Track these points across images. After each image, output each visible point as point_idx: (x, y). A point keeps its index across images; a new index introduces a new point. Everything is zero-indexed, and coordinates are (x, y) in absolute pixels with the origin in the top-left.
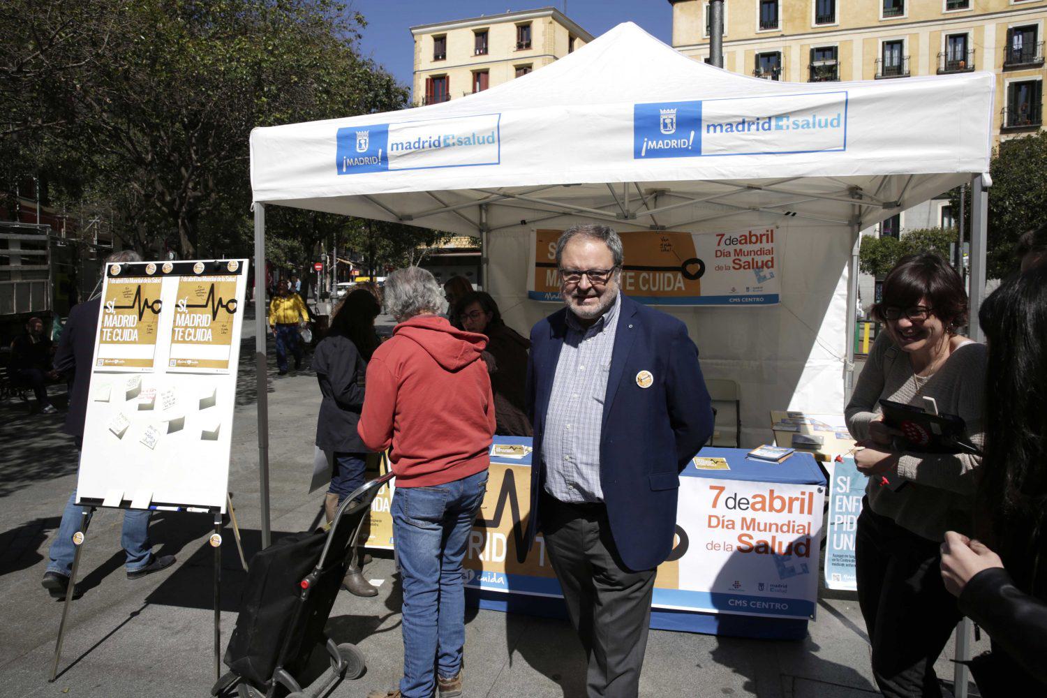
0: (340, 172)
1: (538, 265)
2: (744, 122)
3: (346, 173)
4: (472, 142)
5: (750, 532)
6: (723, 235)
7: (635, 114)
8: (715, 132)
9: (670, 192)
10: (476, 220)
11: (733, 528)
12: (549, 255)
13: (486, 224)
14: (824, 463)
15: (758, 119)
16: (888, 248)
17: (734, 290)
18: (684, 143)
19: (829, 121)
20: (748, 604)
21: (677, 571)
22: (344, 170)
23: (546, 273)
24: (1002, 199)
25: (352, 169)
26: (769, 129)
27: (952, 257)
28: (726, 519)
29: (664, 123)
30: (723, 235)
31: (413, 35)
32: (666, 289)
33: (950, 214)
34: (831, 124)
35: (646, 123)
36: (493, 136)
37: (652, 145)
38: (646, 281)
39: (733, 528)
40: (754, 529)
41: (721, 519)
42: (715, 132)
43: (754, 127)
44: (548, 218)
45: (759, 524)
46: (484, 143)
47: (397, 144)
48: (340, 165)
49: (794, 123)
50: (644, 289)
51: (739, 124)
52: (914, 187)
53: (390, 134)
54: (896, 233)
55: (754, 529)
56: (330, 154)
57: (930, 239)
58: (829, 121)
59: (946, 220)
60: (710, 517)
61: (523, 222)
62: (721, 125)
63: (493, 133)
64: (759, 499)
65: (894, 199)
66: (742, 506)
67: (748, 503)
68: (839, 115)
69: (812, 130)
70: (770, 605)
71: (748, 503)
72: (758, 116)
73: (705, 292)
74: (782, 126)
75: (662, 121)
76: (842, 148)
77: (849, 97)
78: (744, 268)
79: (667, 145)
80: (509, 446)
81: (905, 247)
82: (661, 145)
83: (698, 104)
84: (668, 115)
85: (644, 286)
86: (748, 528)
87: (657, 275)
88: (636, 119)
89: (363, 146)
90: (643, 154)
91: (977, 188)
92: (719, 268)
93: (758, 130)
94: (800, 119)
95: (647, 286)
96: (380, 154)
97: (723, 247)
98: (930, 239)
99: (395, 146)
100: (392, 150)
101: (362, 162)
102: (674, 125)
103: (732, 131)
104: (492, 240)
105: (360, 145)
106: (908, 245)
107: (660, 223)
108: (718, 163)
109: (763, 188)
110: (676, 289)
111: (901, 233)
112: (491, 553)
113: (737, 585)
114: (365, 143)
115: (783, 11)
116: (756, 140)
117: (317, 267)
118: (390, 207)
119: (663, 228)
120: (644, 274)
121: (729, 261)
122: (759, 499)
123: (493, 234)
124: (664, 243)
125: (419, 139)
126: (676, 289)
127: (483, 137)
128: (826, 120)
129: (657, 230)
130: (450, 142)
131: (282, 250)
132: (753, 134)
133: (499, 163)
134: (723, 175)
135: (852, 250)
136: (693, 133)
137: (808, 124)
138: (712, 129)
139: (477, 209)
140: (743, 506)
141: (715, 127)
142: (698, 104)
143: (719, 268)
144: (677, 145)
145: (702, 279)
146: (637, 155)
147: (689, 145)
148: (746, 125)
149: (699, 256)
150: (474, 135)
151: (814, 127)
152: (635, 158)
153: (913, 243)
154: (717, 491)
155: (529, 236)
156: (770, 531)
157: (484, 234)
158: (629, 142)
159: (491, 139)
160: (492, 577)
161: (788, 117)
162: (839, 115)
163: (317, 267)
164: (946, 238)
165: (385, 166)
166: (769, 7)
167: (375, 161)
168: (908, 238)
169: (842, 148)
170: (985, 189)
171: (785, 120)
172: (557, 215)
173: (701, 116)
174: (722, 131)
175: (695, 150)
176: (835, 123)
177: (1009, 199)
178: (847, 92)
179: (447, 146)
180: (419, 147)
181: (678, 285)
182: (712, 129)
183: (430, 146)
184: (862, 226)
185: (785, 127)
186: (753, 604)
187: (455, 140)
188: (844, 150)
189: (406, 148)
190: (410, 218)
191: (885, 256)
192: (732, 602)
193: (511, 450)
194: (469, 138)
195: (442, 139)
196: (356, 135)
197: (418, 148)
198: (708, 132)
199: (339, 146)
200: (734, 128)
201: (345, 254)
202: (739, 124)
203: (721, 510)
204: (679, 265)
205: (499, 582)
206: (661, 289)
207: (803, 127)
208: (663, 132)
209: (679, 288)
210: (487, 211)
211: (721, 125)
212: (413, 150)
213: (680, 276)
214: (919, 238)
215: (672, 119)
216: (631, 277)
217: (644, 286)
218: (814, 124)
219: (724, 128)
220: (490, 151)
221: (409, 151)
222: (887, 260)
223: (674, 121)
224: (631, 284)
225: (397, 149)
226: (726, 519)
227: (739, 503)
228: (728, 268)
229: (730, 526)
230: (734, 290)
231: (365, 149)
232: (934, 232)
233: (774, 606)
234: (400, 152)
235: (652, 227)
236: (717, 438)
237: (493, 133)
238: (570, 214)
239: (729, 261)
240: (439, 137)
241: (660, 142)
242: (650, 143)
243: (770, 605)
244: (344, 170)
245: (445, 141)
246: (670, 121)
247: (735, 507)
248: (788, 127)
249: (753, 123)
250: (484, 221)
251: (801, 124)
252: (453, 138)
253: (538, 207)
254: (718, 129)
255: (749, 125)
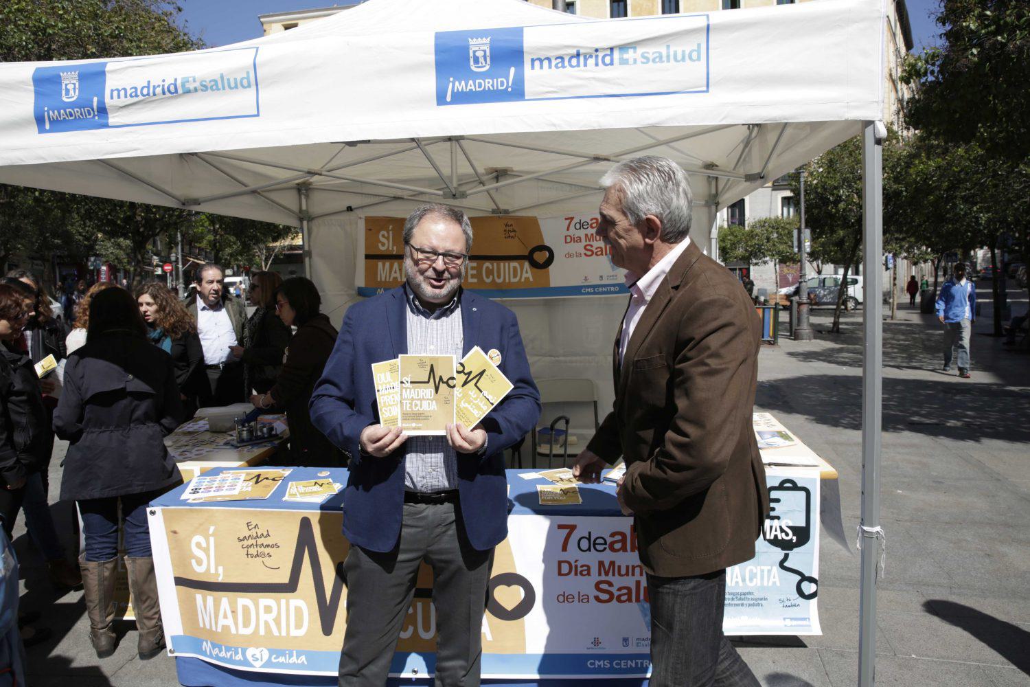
0: (42, 130)
1: (367, 257)
2: (578, 55)
3: (50, 131)
4: (220, 86)
5: (610, 578)
6: (572, 219)
7: (437, 46)
8: (541, 67)
9: (513, 171)
10: (295, 208)
11: (589, 574)
12: (380, 245)
13: (307, 211)
14: (677, 392)
15: (597, 50)
16: (736, 236)
17: (586, 279)
18: (502, 83)
19: (687, 53)
20: (611, 663)
21: (523, 630)
22: (47, 127)
23: (377, 265)
24: (836, 188)
25: (59, 125)
26: (612, 64)
27: (796, 243)
28: (579, 564)
29: (474, 55)
30: (572, 219)
31: (262, 24)
32: (513, 280)
33: (789, 204)
34: (690, 58)
35: (451, 57)
36: (248, 78)
37: (460, 86)
38: (490, 272)
39: (589, 574)
40: (614, 575)
41: (573, 564)
42: (541, 67)
43: (591, 61)
44: (381, 203)
45: (619, 567)
46: (236, 87)
47: (119, 91)
48: (40, 120)
49: (643, 56)
50: (488, 281)
51: (572, 57)
52: (779, 156)
53: (108, 76)
54: (742, 223)
55: (614, 575)
56: (25, 104)
57: (773, 227)
58: (687, 53)
59: (785, 210)
60: (560, 563)
61: (350, 209)
62: (549, 59)
63: (248, 73)
64: (618, 538)
65: (756, 170)
66: (599, 547)
67: (605, 543)
68: (699, 45)
69: (665, 64)
70: (637, 664)
71: (605, 543)
72: (597, 46)
73: (554, 283)
74: (628, 60)
75: (471, 55)
76: (705, 89)
77: (711, 22)
78: (212, 90)
79: (480, 85)
80: (313, 481)
81: (751, 235)
82: (471, 86)
83: (519, 31)
84: (479, 47)
85: (488, 277)
86: (607, 574)
87: (502, 264)
88: (436, 54)
89: (72, 92)
90: (449, 99)
91: (869, 141)
92: (570, 255)
93: (597, 65)
94: (651, 50)
95: (491, 277)
96: (95, 104)
97: (572, 232)
98: (773, 227)
99: (115, 93)
100: (112, 98)
101: (71, 115)
102: (488, 59)
103: (563, 67)
104: (315, 230)
105: (67, 91)
106: (754, 233)
107: (502, 207)
108: (549, 108)
109: (611, 159)
110: (523, 280)
111: (747, 223)
112: (288, 625)
113: (596, 642)
114: (74, 89)
115: (632, 10)
116: (594, 78)
117: (166, 268)
118: (168, 188)
119: (506, 212)
120: (487, 264)
121: (579, 247)
122: (618, 538)
123: (315, 224)
124: (508, 228)
125: (149, 82)
126: (523, 280)
127: (235, 79)
128: (683, 52)
129: (500, 214)
130: (191, 86)
131: (124, 250)
132: (591, 70)
133: (258, 115)
134: (554, 125)
135: (710, 232)
136: (513, 70)
137: (661, 57)
138: (537, 63)
139: (294, 193)
140: (599, 547)
141: (541, 61)
142: (519, 31)
143: (570, 255)
144: (493, 86)
145: (551, 267)
146: (441, 100)
147: (507, 87)
148: (582, 58)
149: (546, 244)
150: (222, 77)
151: (668, 61)
152: (439, 104)
153: (758, 231)
154: (567, 531)
155: (357, 223)
156: (633, 575)
157: (305, 223)
158: (428, 82)
159: (245, 82)
160: (291, 656)
161: (635, 48)
162: (699, 45)
163: (166, 268)
164: (788, 226)
165: (104, 121)
166: (619, 6)
167: (90, 114)
168: (754, 227)
169: (705, 89)
170: (878, 141)
171: (631, 51)
172: (386, 199)
173: (522, 47)
174: (550, 67)
175: (517, 93)
176: (695, 55)
177: (842, 188)
178: (708, 16)
179: (188, 92)
180: (148, 94)
181: (525, 275)
182: (537, 63)
183: (164, 93)
184: (719, 207)
185: (631, 61)
186: (617, 664)
187: (197, 85)
188: (707, 91)
189: (131, 96)
190: (197, 202)
191: (734, 244)
192: (591, 664)
193: (317, 488)
194: (216, 81)
195: (179, 83)
196: (60, 76)
197: (147, 96)
198: (533, 68)
199: (37, 93)
200: (566, 63)
201: (199, 255)
202: (572, 57)
203: (573, 554)
204: (526, 253)
205: (300, 662)
206: (507, 281)
207: (654, 60)
208: (473, 68)
209: (527, 279)
210: (307, 197)
211: (549, 59)
212: (141, 98)
213: (527, 264)
214: (764, 226)
215: (485, 51)
216: (473, 268)
217: (488, 277)
218: (668, 57)
219: (554, 62)
220: (243, 100)
221: (135, 99)
222: (735, 248)
223: (488, 54)
224: (473, 276)
225: (119, 97)
226: (579, 564)
227: (595, 544)
228: (579, 255)
229: (585, 573)
230: (586, 279)
231: (74, 96)
232: (776, 220)
233: (642, 664)
234: (124, 101)
235: (494, 211)
236: (572, 445)
237: (248, 73)
238: (402, 199)
239: (579, 247)
240: (176, 80)
241: (471, 82)
242: (457, 83)
243: (637, 664)
244: (47, 127)
245: (183, 85)
246: (482, 53)
247: (589, 549)
248: (635, 61)
249: (591, 56)
250: (304, 208)
251: (651, 57)
252: (194, 81)
253: (366, 190)
254: (546, 63)
255: (586, 59)
